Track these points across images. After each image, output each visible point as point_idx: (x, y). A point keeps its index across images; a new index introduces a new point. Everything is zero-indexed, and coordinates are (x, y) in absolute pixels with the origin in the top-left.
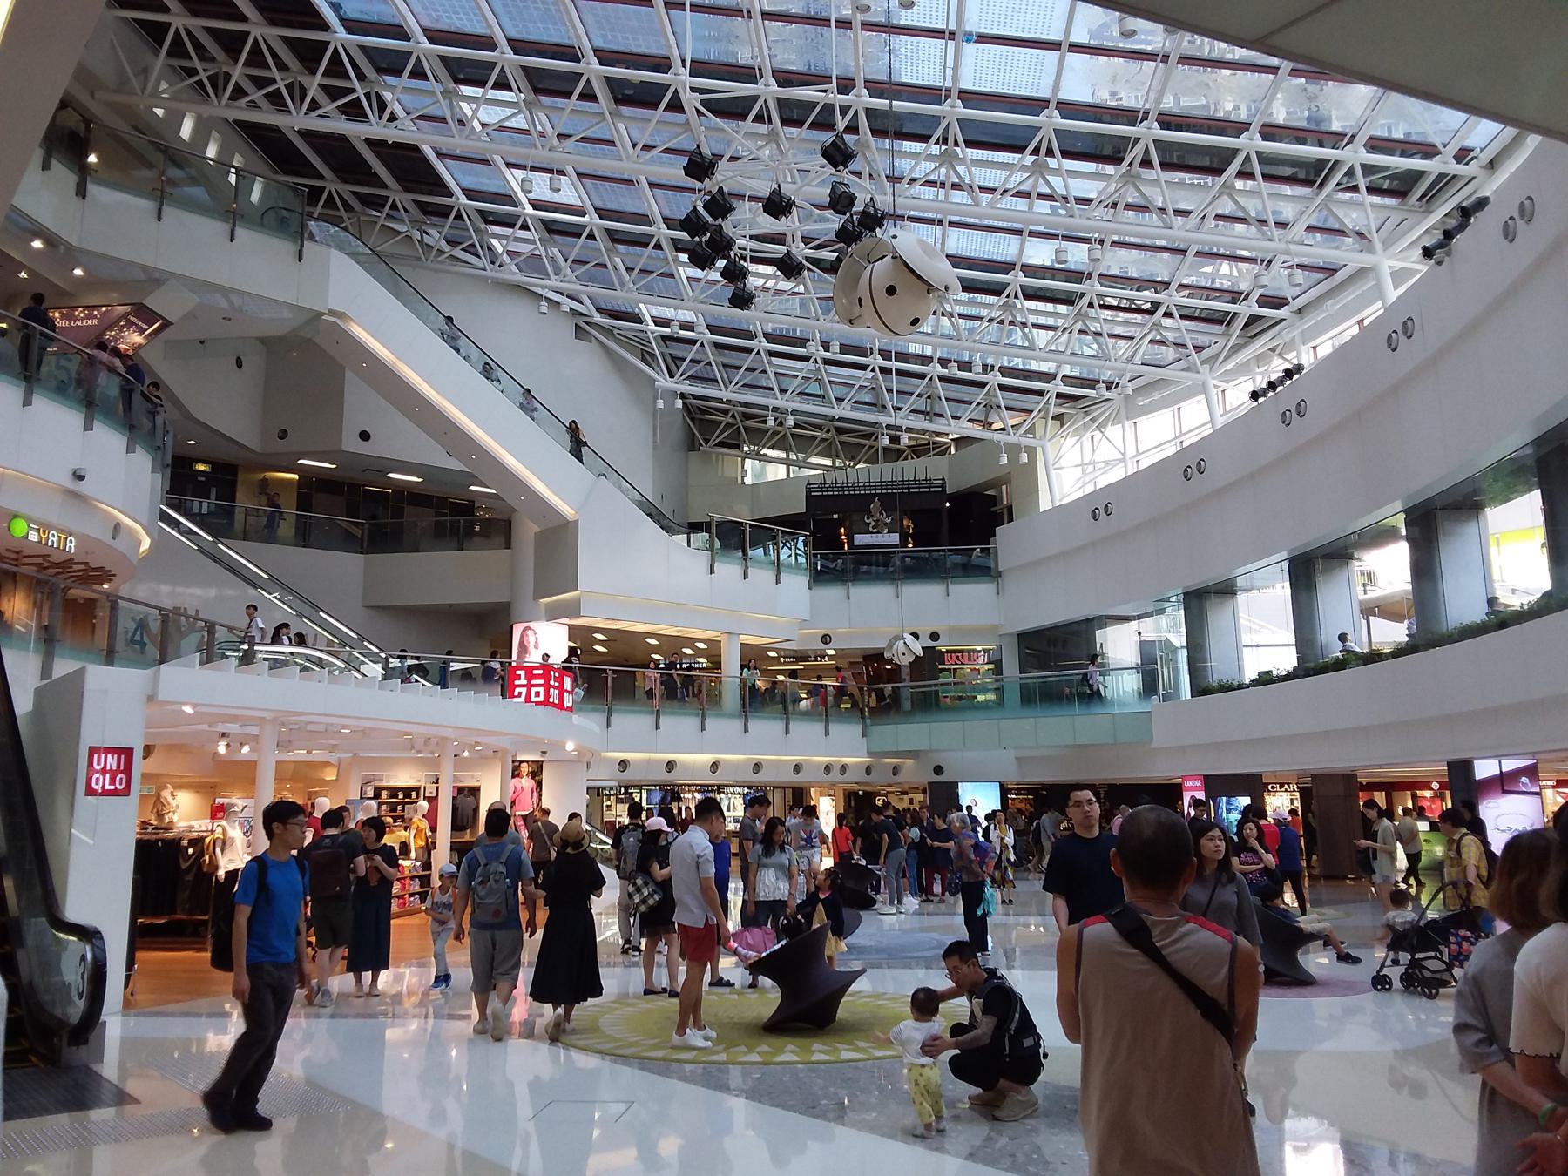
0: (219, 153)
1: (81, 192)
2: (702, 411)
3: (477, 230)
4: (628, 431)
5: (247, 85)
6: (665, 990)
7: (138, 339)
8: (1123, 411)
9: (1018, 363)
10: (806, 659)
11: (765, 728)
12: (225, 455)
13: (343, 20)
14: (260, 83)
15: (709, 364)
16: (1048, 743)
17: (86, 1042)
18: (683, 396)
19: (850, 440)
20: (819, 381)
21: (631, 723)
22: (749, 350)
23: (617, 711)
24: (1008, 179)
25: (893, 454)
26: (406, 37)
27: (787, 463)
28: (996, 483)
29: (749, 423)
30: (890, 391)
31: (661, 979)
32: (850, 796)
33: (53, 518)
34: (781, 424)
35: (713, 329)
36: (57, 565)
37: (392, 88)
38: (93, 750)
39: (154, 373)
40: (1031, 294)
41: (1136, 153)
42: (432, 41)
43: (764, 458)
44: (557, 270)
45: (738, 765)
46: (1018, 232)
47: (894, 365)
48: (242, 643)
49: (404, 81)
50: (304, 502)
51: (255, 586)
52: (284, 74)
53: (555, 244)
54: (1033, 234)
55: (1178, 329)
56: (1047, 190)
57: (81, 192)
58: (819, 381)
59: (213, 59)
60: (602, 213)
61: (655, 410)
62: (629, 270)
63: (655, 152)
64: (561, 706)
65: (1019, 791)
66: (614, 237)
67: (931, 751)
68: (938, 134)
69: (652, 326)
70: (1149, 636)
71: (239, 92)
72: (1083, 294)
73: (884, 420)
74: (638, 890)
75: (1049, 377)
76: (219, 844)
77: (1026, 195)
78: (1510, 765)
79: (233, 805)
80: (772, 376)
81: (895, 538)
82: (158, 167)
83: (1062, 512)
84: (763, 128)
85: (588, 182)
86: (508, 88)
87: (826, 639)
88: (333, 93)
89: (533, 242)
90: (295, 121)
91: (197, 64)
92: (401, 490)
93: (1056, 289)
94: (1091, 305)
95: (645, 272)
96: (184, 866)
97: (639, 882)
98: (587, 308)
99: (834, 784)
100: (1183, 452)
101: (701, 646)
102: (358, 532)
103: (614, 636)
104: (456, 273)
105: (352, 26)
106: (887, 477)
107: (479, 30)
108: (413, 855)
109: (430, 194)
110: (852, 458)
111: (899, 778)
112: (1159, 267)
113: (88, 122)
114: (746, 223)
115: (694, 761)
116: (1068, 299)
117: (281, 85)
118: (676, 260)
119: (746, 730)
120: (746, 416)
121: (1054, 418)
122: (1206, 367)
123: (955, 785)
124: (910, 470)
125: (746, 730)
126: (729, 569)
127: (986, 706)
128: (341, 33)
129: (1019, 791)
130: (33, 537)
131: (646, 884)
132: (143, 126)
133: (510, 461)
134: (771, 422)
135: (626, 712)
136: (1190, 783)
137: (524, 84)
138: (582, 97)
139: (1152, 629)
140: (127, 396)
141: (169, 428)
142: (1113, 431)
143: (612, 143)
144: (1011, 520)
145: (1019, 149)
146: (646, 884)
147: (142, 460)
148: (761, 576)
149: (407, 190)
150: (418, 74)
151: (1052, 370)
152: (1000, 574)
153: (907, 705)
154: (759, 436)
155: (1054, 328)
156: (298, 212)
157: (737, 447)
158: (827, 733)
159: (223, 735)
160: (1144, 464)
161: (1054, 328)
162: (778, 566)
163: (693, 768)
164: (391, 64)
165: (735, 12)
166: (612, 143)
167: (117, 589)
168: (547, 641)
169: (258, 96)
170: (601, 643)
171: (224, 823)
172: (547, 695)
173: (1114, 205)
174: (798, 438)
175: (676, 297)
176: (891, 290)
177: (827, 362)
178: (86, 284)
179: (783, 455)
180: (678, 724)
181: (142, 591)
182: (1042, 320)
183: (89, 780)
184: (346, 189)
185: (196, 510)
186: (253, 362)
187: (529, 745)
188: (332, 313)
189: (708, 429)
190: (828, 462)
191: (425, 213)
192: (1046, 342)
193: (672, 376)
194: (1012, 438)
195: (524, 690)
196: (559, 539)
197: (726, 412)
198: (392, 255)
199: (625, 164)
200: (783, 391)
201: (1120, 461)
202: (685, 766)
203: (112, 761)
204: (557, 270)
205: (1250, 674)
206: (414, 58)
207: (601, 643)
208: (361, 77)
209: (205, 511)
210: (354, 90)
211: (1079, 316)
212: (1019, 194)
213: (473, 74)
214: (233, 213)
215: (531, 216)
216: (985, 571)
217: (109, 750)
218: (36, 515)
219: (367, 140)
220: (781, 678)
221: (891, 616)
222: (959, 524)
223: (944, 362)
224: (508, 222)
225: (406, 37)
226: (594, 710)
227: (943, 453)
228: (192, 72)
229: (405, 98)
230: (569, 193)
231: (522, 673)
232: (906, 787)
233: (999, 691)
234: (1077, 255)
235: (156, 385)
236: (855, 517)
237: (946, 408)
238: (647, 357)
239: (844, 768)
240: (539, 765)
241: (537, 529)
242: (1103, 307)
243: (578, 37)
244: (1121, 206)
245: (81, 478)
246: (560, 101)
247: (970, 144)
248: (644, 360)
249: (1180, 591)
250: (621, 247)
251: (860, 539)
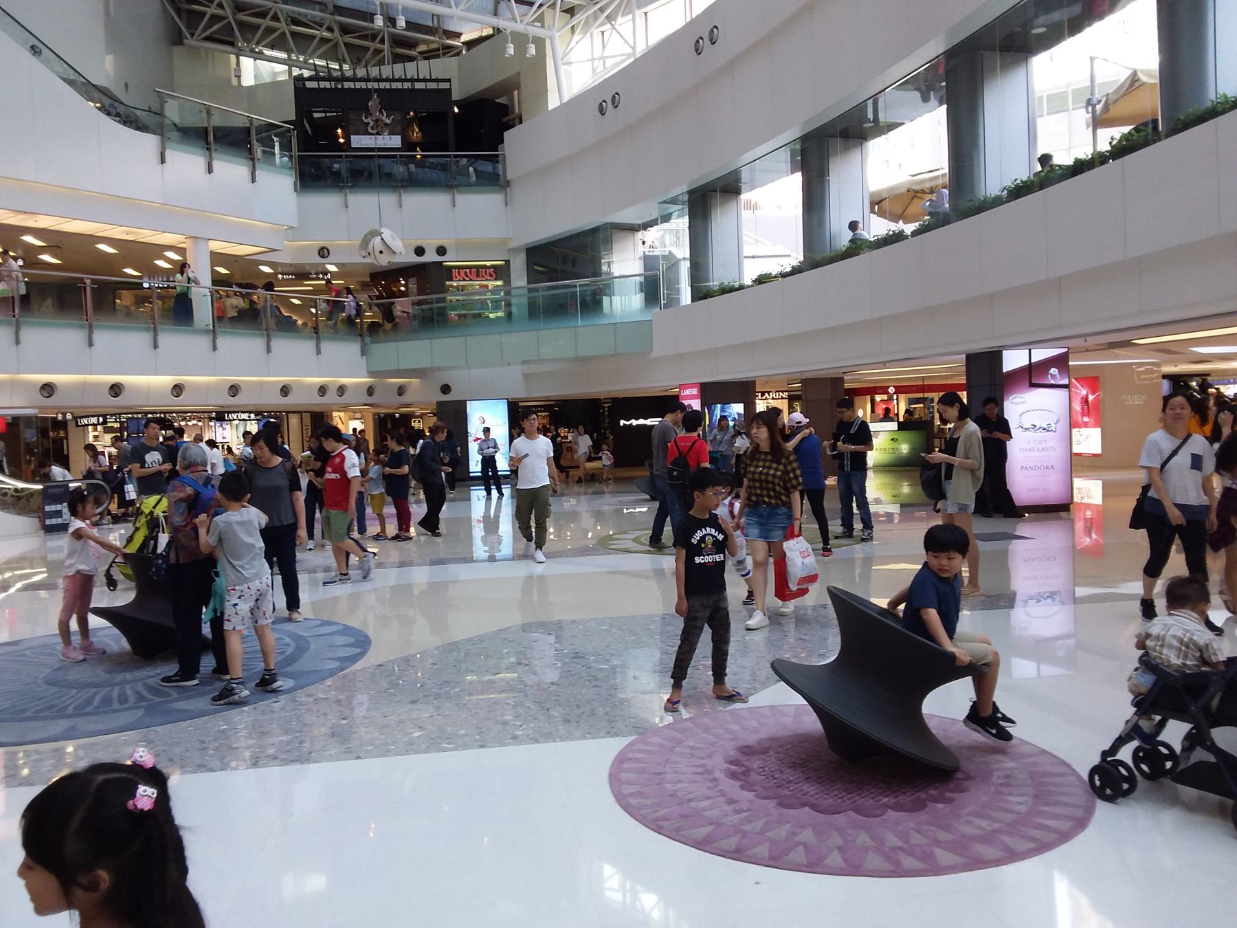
16: (560, 357)
23: (100, 327)
43: (258, 56)
45: (207, 388)
78: (1040, 355)
87: (323, 252)
111: (406, 399)
123: (465, 402)
136: (687, 392)
142: (623, 22)
157: (232, 44)
158: (318, 352)
163: (148, 391)
179: (284, 56)
202: (136, 389)
205: (750, 273)
216: (494, 180)
222: (467, 130)
227: (458, 54)
236: (352, 116)
239: (342, 390)
251: (358, 141)
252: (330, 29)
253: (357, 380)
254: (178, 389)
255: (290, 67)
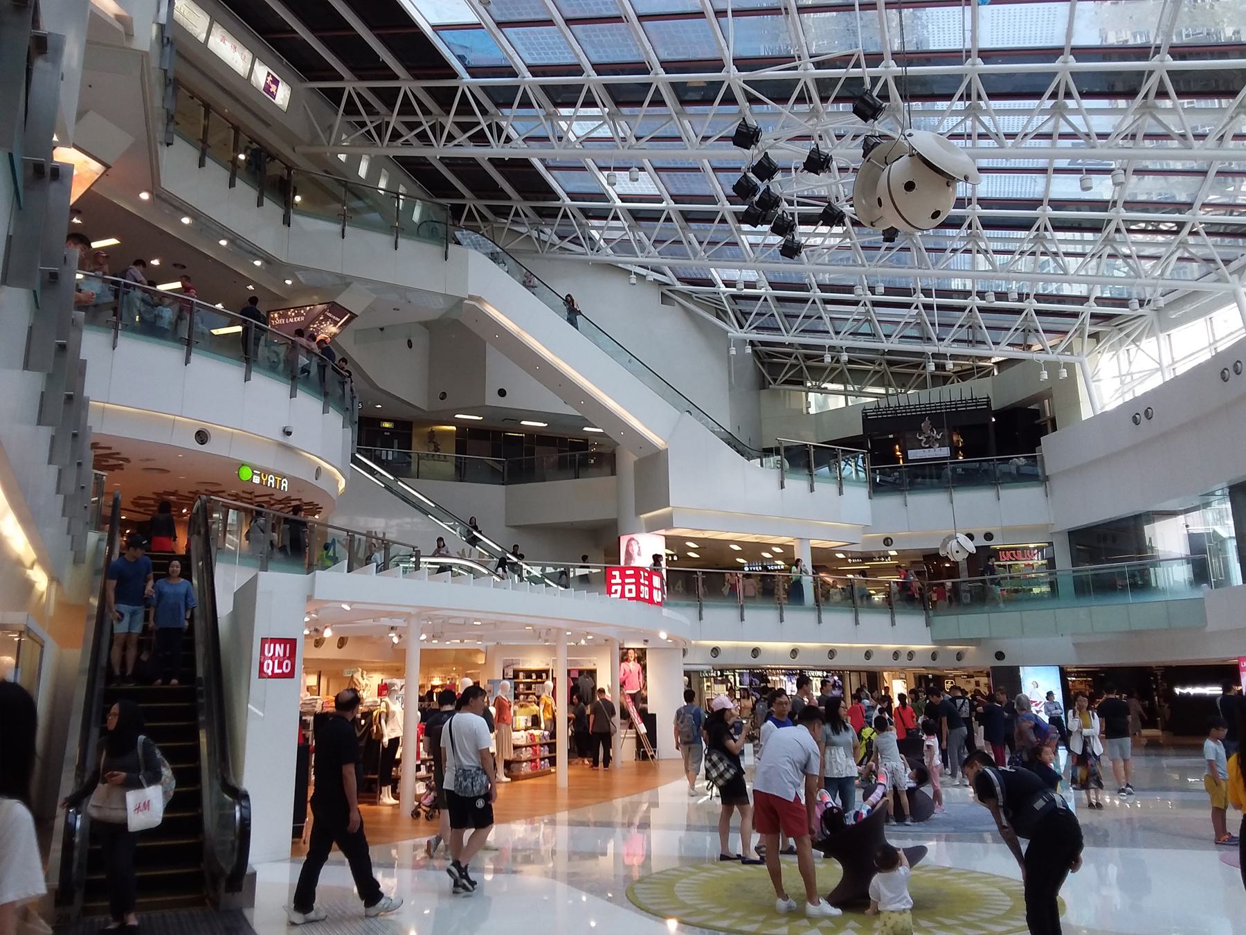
0: (388, 184)
1: (287, 221)
2: (770, 355)
3: (580, 225)
4: (709, 377)
5: (402, 129)
6: (739, 856)
7: (333, 329)
8: (1156, 325)
9: (1052, 289)
10: (871, 559)
11: (837, 619)
12: (404, 414)
13: (467, 68)
14: (411, 126)
15: (773, 315)
16: (1111, 631)
17: (240, 889)
18: (752, 343)
19: (900, 369)
20: (869, 321)
21: (720, 616)
22: (805, 301)
23: (707, 606)
24: (1029, 121)
25: (941, 379)
26: (515, 75)
27: (846, 394)
28: (1038, 398)
29: (810, 363)
30: (933, 324)
31: (736, 847)
32: (921, 679)
33: (268, 464)
34: (838, 361)
35: (774, 286)
36: (280, 502)
37: (505, 117)
38: (264, 641)
39: (342, 351)
40: (1060, 226)
41: (1151, 84)
42: (534, 75)
44: (643, 249)
46: (1043, 171)
47: (935, 301)
48: (411, 556)
49: (515, 111)
50: (461, 448)
51: (427, 513)
52: (428, 118)
53: (641, 228)
54: (1058, 171)
55: (1205, 246)
56: (1069, 130)
57: (287, 221)
58: (869, 321)
59: (378, 113)
60: (677, 199)
61: (729, 357)
62: (701, 243)
63: (711, 141)
64: (651, 601)
65: (1078, 674)
66: (688, 217)
67: (991, 638)
68: (962, 89)
69: (723, 288)
70: (1197, 528)
71: (396, 135)
72: (1109, 221)
73: (929, 349)
74: (714, 765)
75: (1082, 300)
76: (383, 716)
77: (1048, 136)
79: (393, 685)
80: (827, 321)
81: (945, 452)
82: (343, 199)
83: (1104, 419)
84: (804, 108)
85: (663, 174)
86: (595, 105)
87: (888, 541)
88: (464, 127)
89: (623, 229)
90: (436, 152)
91: (365, 118)
92: (533, 434)
93: (1084, 219)
94: (1118, 230)
95: (713, 243)
96: (358, 734)
97: (715, 758)
98: (670, 278)
99: (903, 669)
100: (1218, 357)
101: (778, 550)
102: (499, 467)
103: (704, 544)
104: (564, 260)
105: (474, 72)
106: (935, 399)
107: (569, 60)
108: (543, 726)
109: (544, 200)
110: (903, 386)
111: (963, 663)
112: (1179, 190)
113: (289, 169)
114: (792, 187)
115: (776, 647)
116: (1096, 227)
117: (426, 126)
118: (739, 230)
119: (820, 622)
120: (808, 357)
121: (1089, 336)
122: (1235, 276)
123: (1018, 668)
124: (955, 392)
125: (820, 622)
126: (797, 485)
127: (1040, 597)
128: (467, 78)
129: (1078, 674)
130: (256, 480)
131: (721, 760)
132: (330, 168)
133: (611, 404)
134: (828, 359)
135: (718, 607)
137: (607, 99)
138: (652, 104)
139: (1199, 522)
140: (324, 373)
141: (357, 395)
142: (1149, 344)
143: (679, 139)
144: (1054, 429)
145: (1037, 95)
146: (721, 760)
147: (335, 419)
148: (826, 489)
149: (526, 199)
150: (526, 103)
151: (1085, 293)
152: (1047, 478)
153: (966, 597)
154: (819, 373)
155: (1083, 255)
156: (446, 227)
157: (802, 383)
158: (893, 624)
159: (392, 628)
160: (1179, 372)
161: (1083, 255)
162: (841, 482)
163: (775, 654)
164: (503, 98)
165: (774, 11)
166: (679, 139)
167: (326, 519)
168: (645, 547)
169: (410, 136)
170: (693, 550)
171: (387, 699)
172: (638, 591)
173: (1133, 136)
174: (853, 371)
175: (739, 260)
176: (910, 186)
177: (876, 304)
178: (299, 289)
179: (841, 387)
180: (762, 616)
181: (339, 521)
182: (1071, 248)
183: (261, 665)
184: (481, 204)
185: (384, 457)
186: (420, 341)
187: (634, 635)
188: (471, 298)
189: (776, 369)
190: (882, 391)
191: (541, 216)
192: (1076, 269)
193: (741, 327)
194: (1051, 357)
195: (619, 588)
196: (653, 464)
197: (789, 355)
198: (517, 251)
199: (690, 151)
200: (837, 333)
201: (1157, 370)
202: (768, 651)
203: (279, 650)
204: (643, 249)
206: (521, 90)
207: (693, 550)
208: (484, 112)
209: (390, 458)
210: (479, 123)
211: (1108, 241)
212: (1039, 136)
213: (563, 97)
214: (397, 228)
215: (620, 208)
216: (1033, 476)
217: (275, 641)
218: (258, 463)
219: (490, 160)
220: (850, 576)
221: (948, 520)
222: (1007, 435)
223: (982, 295)
224: (602, 215)
225: (515, 75)
226: (688, 605)
228: (363, 125)
229: (517, 124)
230: (646, 184)
231: (616, 573)
232: (971, 671)
233: (1053, 585)
234: (1102, 188)
235: (344, 360)
236: (908, 436)
237: (987, 335)
238: (720, 314)
239: (911, 654)
240: (643, 651)
241: (636, 458)
242: (1129, 231)
243: (647, 53)
244: (1140, 136)
245: (289, 433)
246: (636, 110)
247: (992, 96)
248: (718, 317)
249: (1225, 485)
250: (693, 225)
251: (913, 454)
252: (880, 364)
253: (923, 647)
254: (794, 652)
255: (846, 396)
